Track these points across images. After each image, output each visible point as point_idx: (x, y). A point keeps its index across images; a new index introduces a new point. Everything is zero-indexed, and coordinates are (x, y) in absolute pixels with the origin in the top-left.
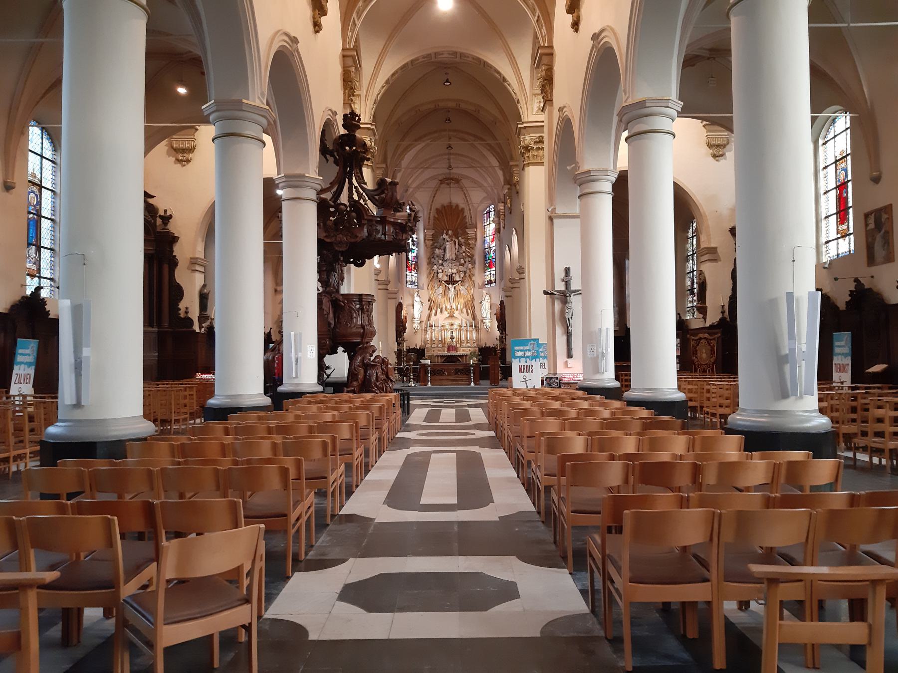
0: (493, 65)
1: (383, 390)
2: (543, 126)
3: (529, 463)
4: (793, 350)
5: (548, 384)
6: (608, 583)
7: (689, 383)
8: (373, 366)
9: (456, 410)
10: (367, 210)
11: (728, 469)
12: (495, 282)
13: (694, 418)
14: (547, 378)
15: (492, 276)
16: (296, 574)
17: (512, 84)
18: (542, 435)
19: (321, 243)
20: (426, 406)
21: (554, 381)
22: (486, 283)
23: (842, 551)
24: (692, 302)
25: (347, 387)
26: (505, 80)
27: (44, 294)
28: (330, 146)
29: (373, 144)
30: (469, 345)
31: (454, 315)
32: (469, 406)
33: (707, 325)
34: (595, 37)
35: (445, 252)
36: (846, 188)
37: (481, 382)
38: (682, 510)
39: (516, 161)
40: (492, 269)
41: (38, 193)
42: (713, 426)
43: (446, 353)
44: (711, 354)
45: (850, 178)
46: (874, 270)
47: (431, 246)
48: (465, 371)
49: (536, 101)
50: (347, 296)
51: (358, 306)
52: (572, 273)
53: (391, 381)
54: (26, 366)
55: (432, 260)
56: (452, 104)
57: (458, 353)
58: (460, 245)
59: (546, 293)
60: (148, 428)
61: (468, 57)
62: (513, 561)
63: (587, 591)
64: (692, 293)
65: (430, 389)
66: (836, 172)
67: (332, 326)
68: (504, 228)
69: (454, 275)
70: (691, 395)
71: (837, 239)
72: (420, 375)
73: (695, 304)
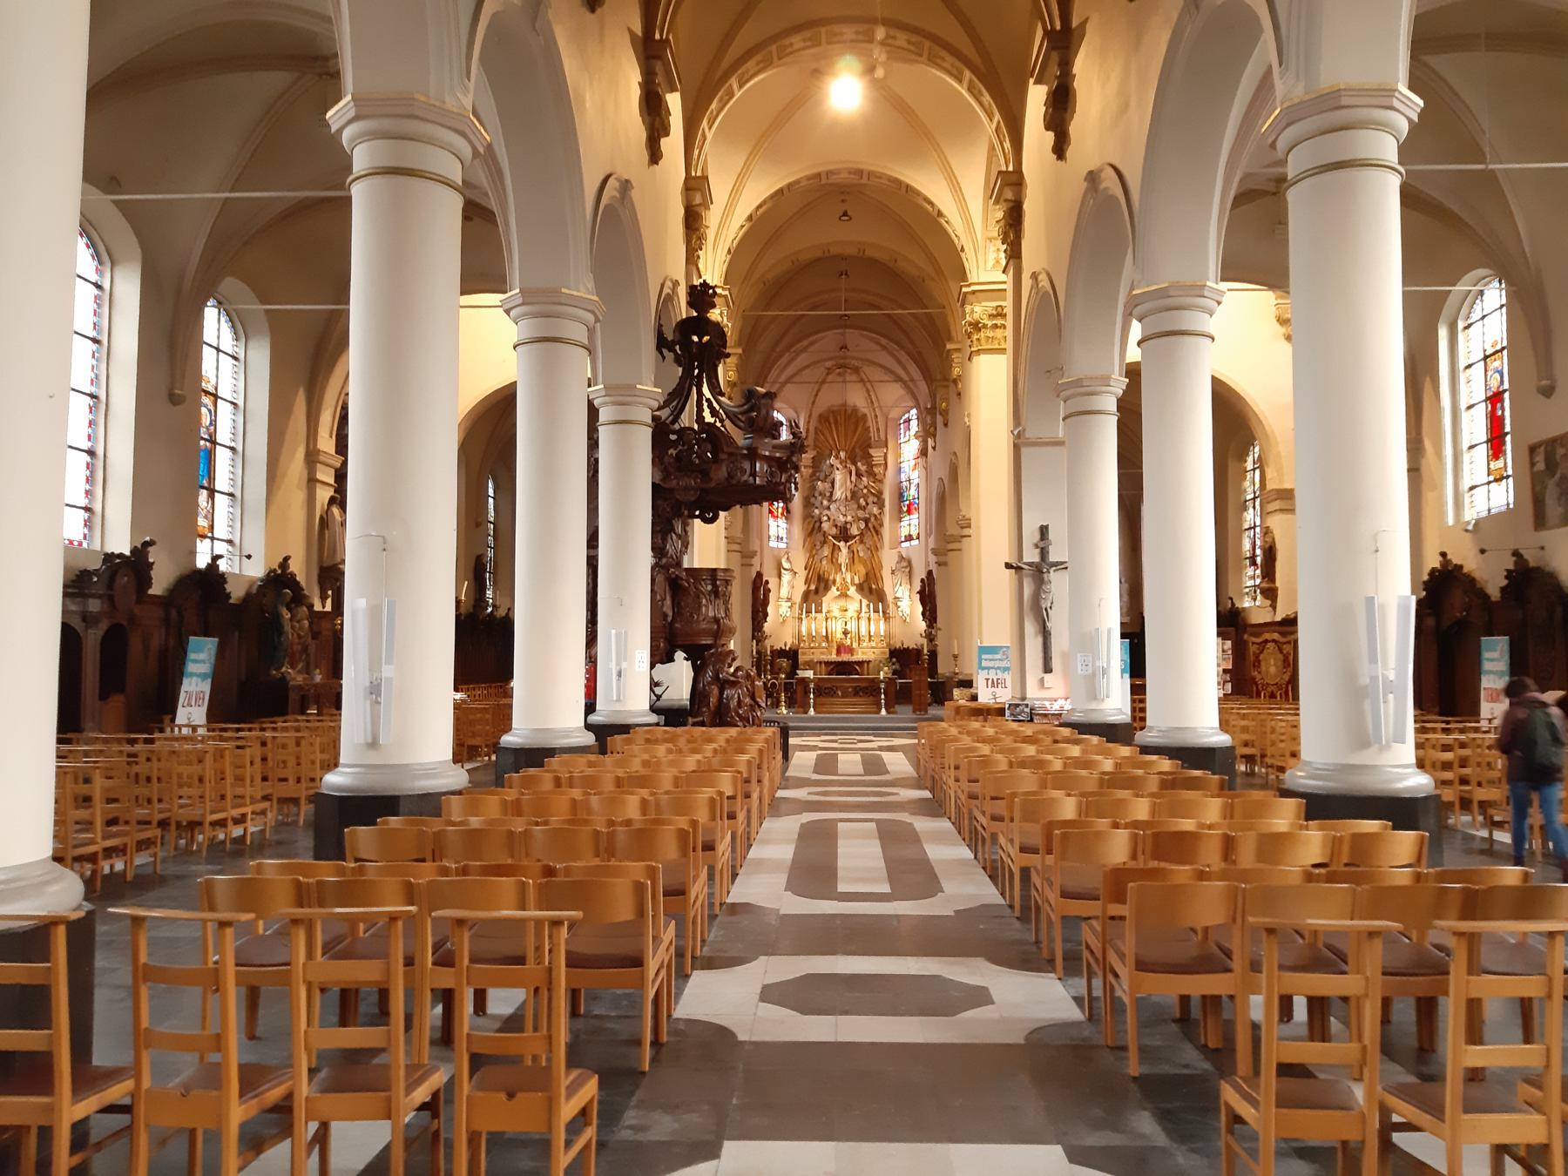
0: (923, 191)
1: (749, 722)
2: (1005, 290)
3: (994, 837)
4: (1374, 679)
5: (1012, 714)
6: (1111, 978)
7: (1244, 717)
8: (734, 684)
9: (862, 756)
10: (728, 438)
11: (1273, 846)
12: (918, 538)
13: (1251, 774)
14: (1010, 705)
15: (913, 528)
16: (695, 972)
17: (952, 221)
18: (1014, 795)
19: (656, 488)
20: (814, 748)
21: (1023, 711)
22: (903, 539)
23: (1407, 944)
24: (1253, 578)
25: (693, 717)
26: (940, 214)
27: (223, 566)
28: (670, 336)
29: (725, 319)
30: (873, 644)
31: (848, 593)
32: (881, 749)
33: (1278, 618)
34: (1092, 177)
35: (833, 487)
36: (1502, 401)
37: (898, 708)
38: (1200, 883)
39: (958, 342)
40: (912, 516)
41: (212, 408)
42: (1265, 786)
43: (833, 657)
44: (1284, 667)
45: (1506, 386)
46: (1546, 536)
47: (811, 476)
48: (869, 690)
49: (992, 249)
50: (693, 572)
51: (709, 588)
52: (1051, 535)
53: (760, 706)
54: (199, 680)
55: (812, 500)
56: (851, 251)
57: (855, 658)
58: (859, 475)
59: (1008, 566)
60: (457, 777)
61: (880, 178)
62: (981, 963)
63: (1083, 998)
64: (1254, 563)
65: (812, 719)
66: (1486, 375)
67: (670, 619)
68: (934, 448)
69: (848, 526)
70: (1245, 737)
71: (1489, 483)
72: (796, 694)
73: (1258, 581)
